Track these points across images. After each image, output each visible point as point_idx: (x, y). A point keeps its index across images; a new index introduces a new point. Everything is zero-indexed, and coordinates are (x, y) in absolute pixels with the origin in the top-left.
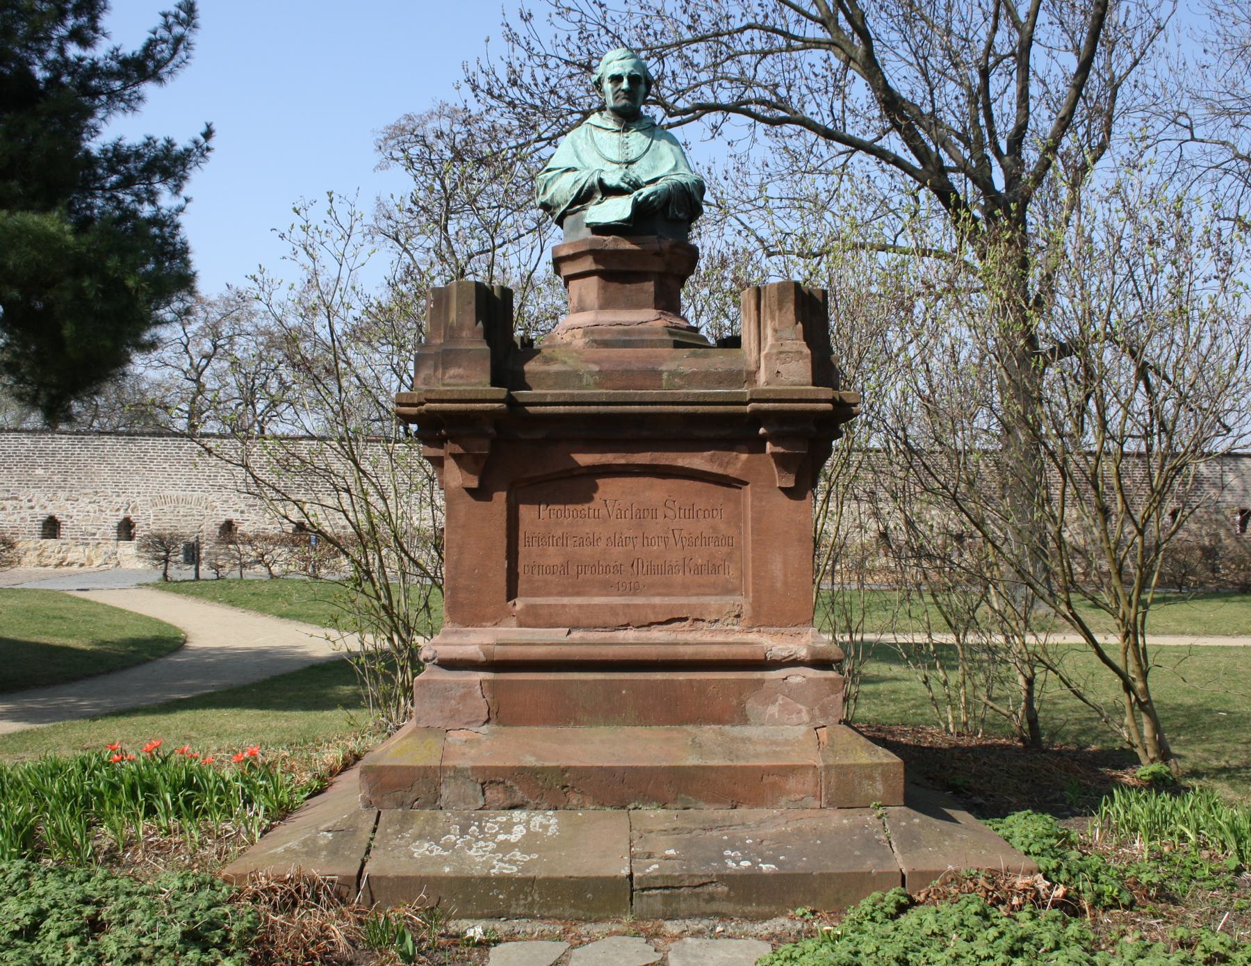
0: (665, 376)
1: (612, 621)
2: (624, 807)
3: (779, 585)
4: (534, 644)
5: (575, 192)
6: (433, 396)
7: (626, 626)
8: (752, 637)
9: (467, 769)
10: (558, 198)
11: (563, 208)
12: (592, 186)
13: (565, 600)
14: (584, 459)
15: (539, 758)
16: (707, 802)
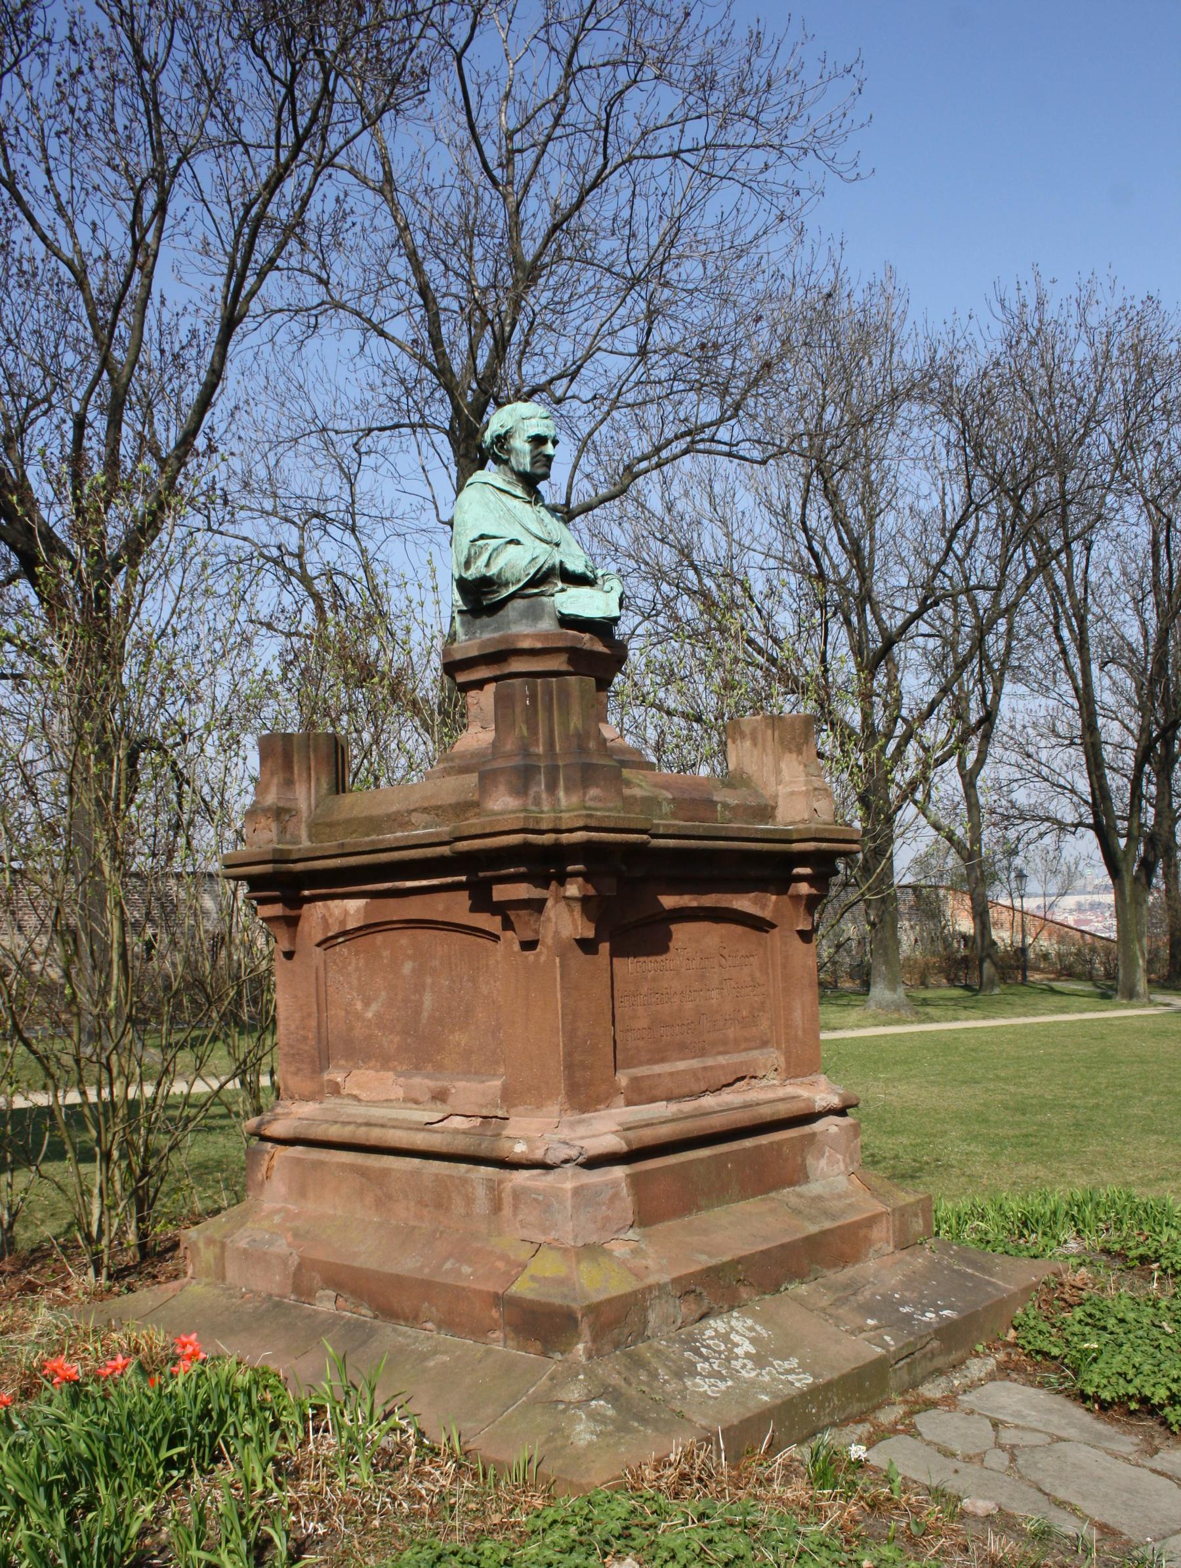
0: (719, 807)
1: (696, 1088)
2: (778, 1291)
3: (800, 1033)
4: (375, 1125)
5: (532, 571)
6: (593, 823)
7: (704, 1093)
8: (790, 1090)
9: (666, 1284)
10: (508, 575)
11: (512, 589)
12: (552, 569)
13: (657, 1069)
14: (669, 901)
15: (710, 1255)
16: (829, 1268)
